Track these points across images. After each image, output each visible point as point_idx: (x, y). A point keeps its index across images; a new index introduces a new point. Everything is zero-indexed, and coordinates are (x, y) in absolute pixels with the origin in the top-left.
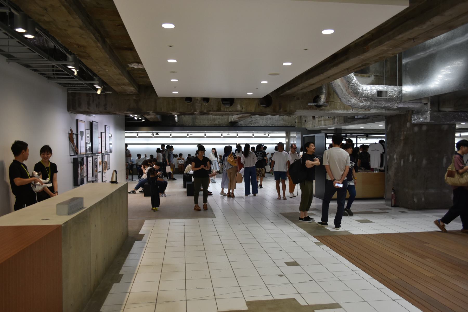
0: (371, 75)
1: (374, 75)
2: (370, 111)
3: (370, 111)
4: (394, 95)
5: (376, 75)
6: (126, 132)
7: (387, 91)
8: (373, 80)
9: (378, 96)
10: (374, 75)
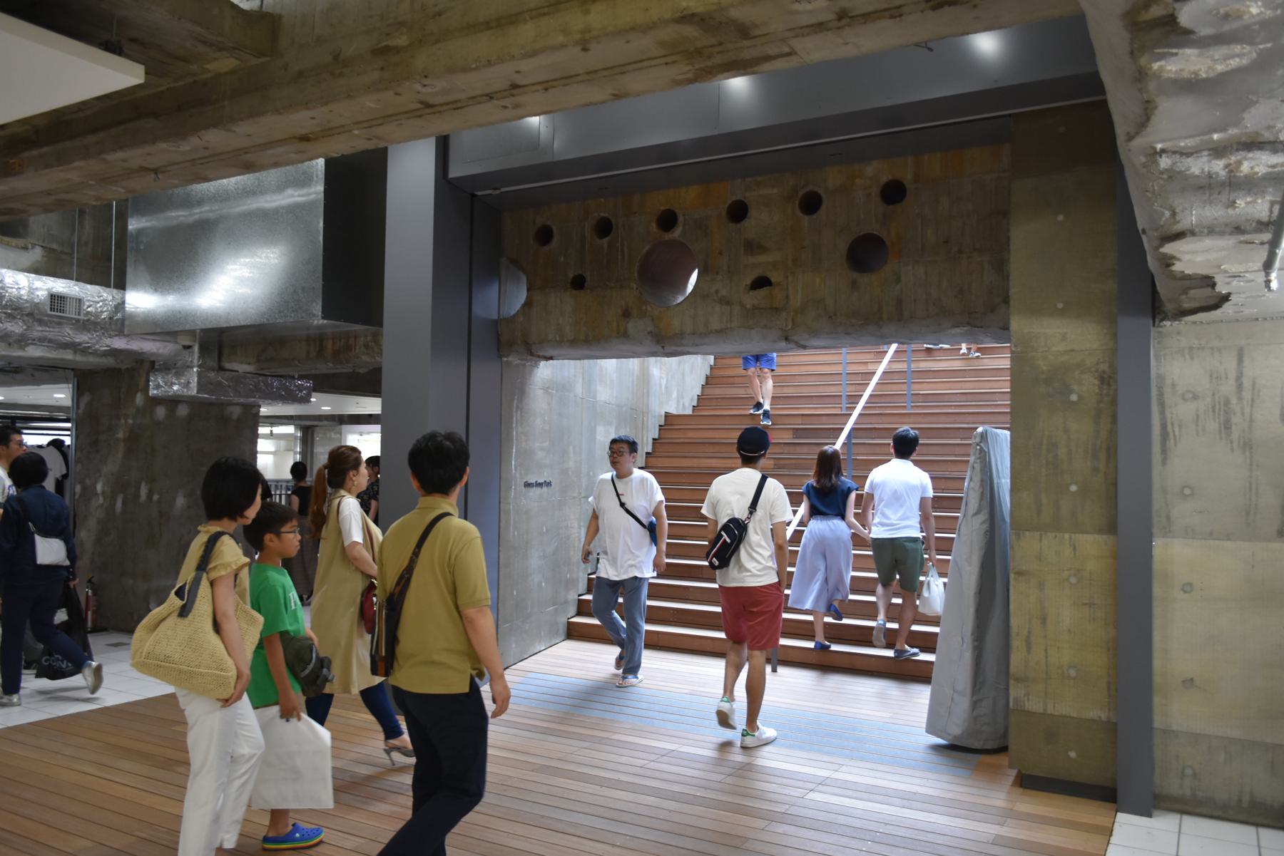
0: (32, 244)
1: (42, 247)
2: (24, 349)
3: (24, 349)
4: (102, 312)
5: (50, 249)
6: (810, 618)
7: (80, 300)
8: (38, 261)
9: (51, 311)
10: (44, 245)
